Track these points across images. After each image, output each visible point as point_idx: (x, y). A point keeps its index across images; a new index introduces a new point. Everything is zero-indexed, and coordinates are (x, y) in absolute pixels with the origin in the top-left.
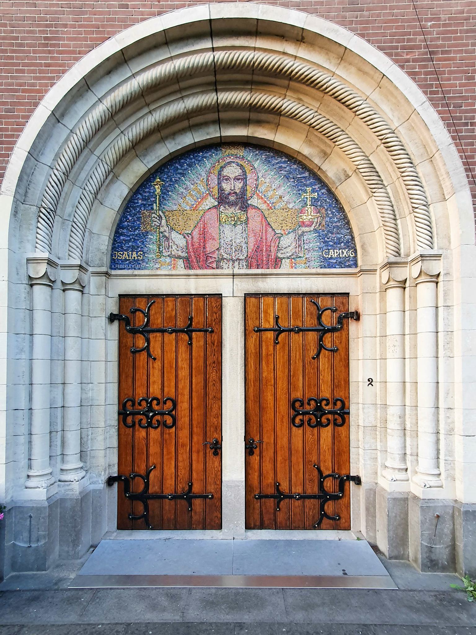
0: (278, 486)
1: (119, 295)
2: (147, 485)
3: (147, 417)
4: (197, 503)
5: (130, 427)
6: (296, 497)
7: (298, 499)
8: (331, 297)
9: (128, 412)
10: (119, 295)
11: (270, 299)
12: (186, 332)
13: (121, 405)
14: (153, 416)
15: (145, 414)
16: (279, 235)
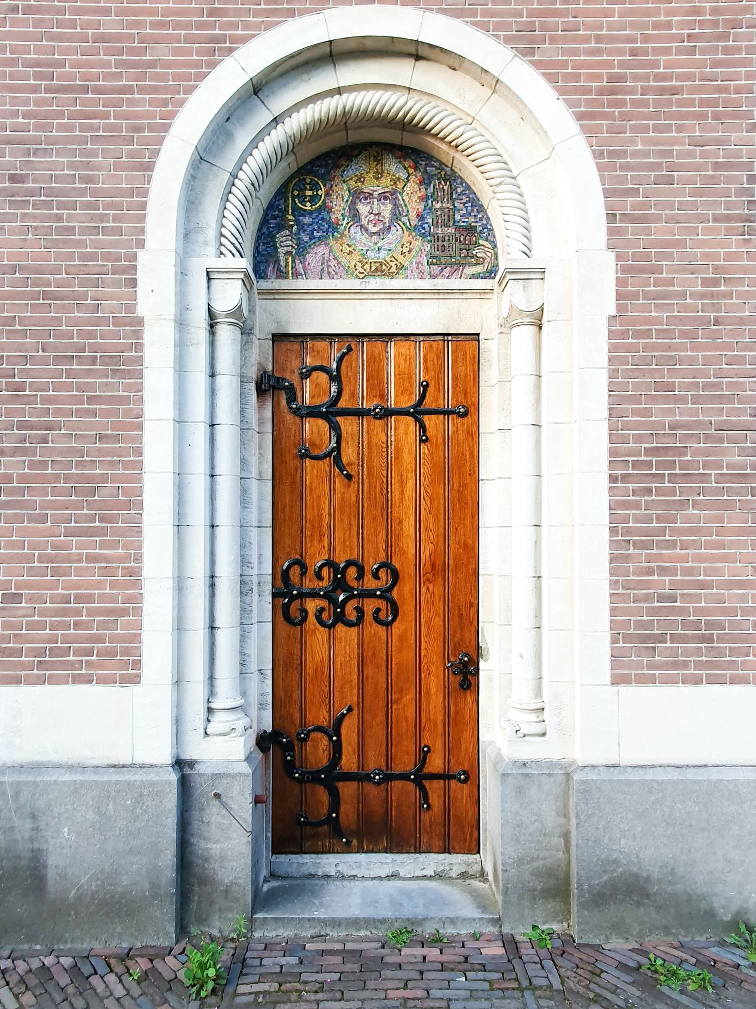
0: (426, 753)
1: (274, 335)
2: (337, 748)
3: (333, 601)
4: (435, 788)
5: (296, 624)
6: (374, 778)
7: (378, 783)
8: (444, 341)
9: (295, 592)
10: (274, 335)
11: (405, 347)
12: (325, 416)
13: (279, 576)
14: (345, 601)
15: (329, 596)
16: (367, 195)
